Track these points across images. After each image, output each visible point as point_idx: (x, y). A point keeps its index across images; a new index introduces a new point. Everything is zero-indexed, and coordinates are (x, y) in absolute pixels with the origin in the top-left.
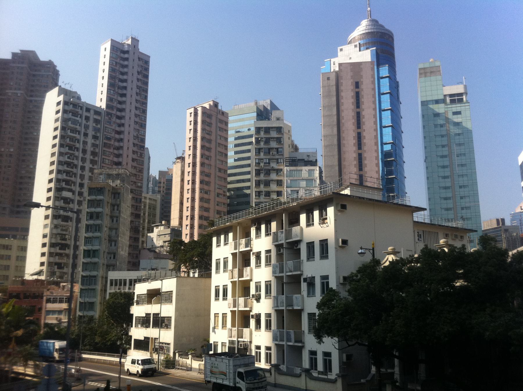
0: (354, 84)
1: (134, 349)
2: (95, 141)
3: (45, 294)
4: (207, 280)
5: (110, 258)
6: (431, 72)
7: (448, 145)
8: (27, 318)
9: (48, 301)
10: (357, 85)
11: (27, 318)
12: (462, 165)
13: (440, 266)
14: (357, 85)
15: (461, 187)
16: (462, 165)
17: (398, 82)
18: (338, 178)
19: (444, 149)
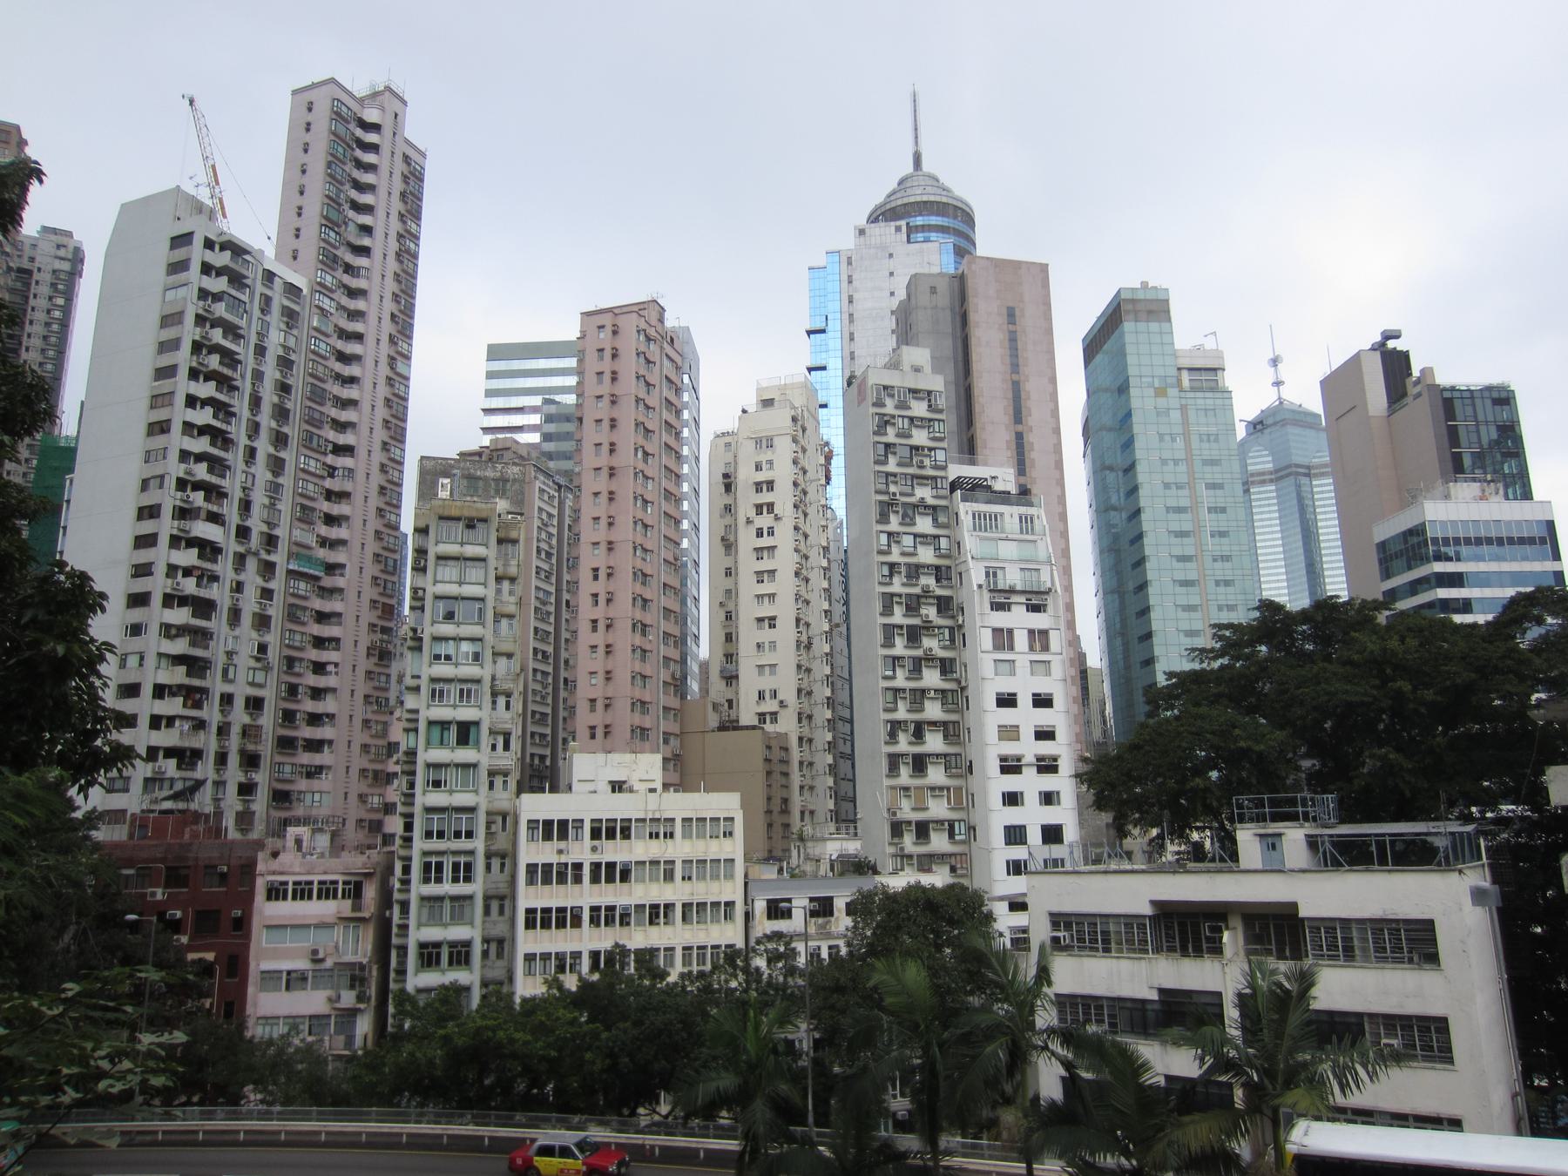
0: (1005, 311)
1: (203, 677)
2: (189, 473)
3: (260, 867)
4: (1507, 1118)
5: (494, 747)
6: (1150, 312)
7: (1190, 485)
8: (191, 956)
9: (275, 893)
10: (1011, 315)
11: (191, 956)
12: (1223, 534)
13: (1220, 778)
14: (1011, 315)
15: (1217, 583)
16: (1223, 534)
17: (461, 454)
18: (1515, 535)
19: (1181, 492)
